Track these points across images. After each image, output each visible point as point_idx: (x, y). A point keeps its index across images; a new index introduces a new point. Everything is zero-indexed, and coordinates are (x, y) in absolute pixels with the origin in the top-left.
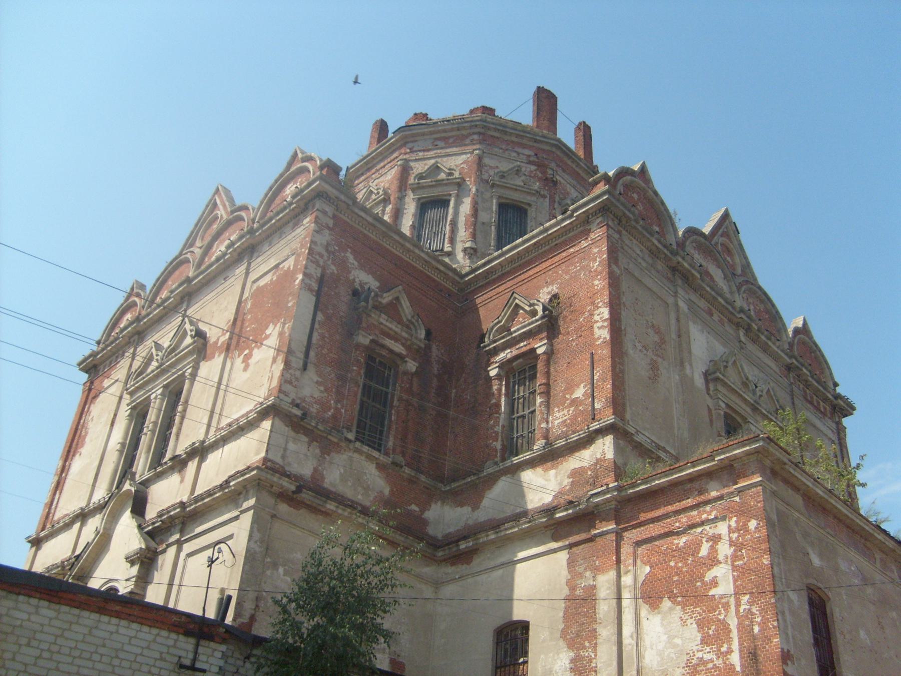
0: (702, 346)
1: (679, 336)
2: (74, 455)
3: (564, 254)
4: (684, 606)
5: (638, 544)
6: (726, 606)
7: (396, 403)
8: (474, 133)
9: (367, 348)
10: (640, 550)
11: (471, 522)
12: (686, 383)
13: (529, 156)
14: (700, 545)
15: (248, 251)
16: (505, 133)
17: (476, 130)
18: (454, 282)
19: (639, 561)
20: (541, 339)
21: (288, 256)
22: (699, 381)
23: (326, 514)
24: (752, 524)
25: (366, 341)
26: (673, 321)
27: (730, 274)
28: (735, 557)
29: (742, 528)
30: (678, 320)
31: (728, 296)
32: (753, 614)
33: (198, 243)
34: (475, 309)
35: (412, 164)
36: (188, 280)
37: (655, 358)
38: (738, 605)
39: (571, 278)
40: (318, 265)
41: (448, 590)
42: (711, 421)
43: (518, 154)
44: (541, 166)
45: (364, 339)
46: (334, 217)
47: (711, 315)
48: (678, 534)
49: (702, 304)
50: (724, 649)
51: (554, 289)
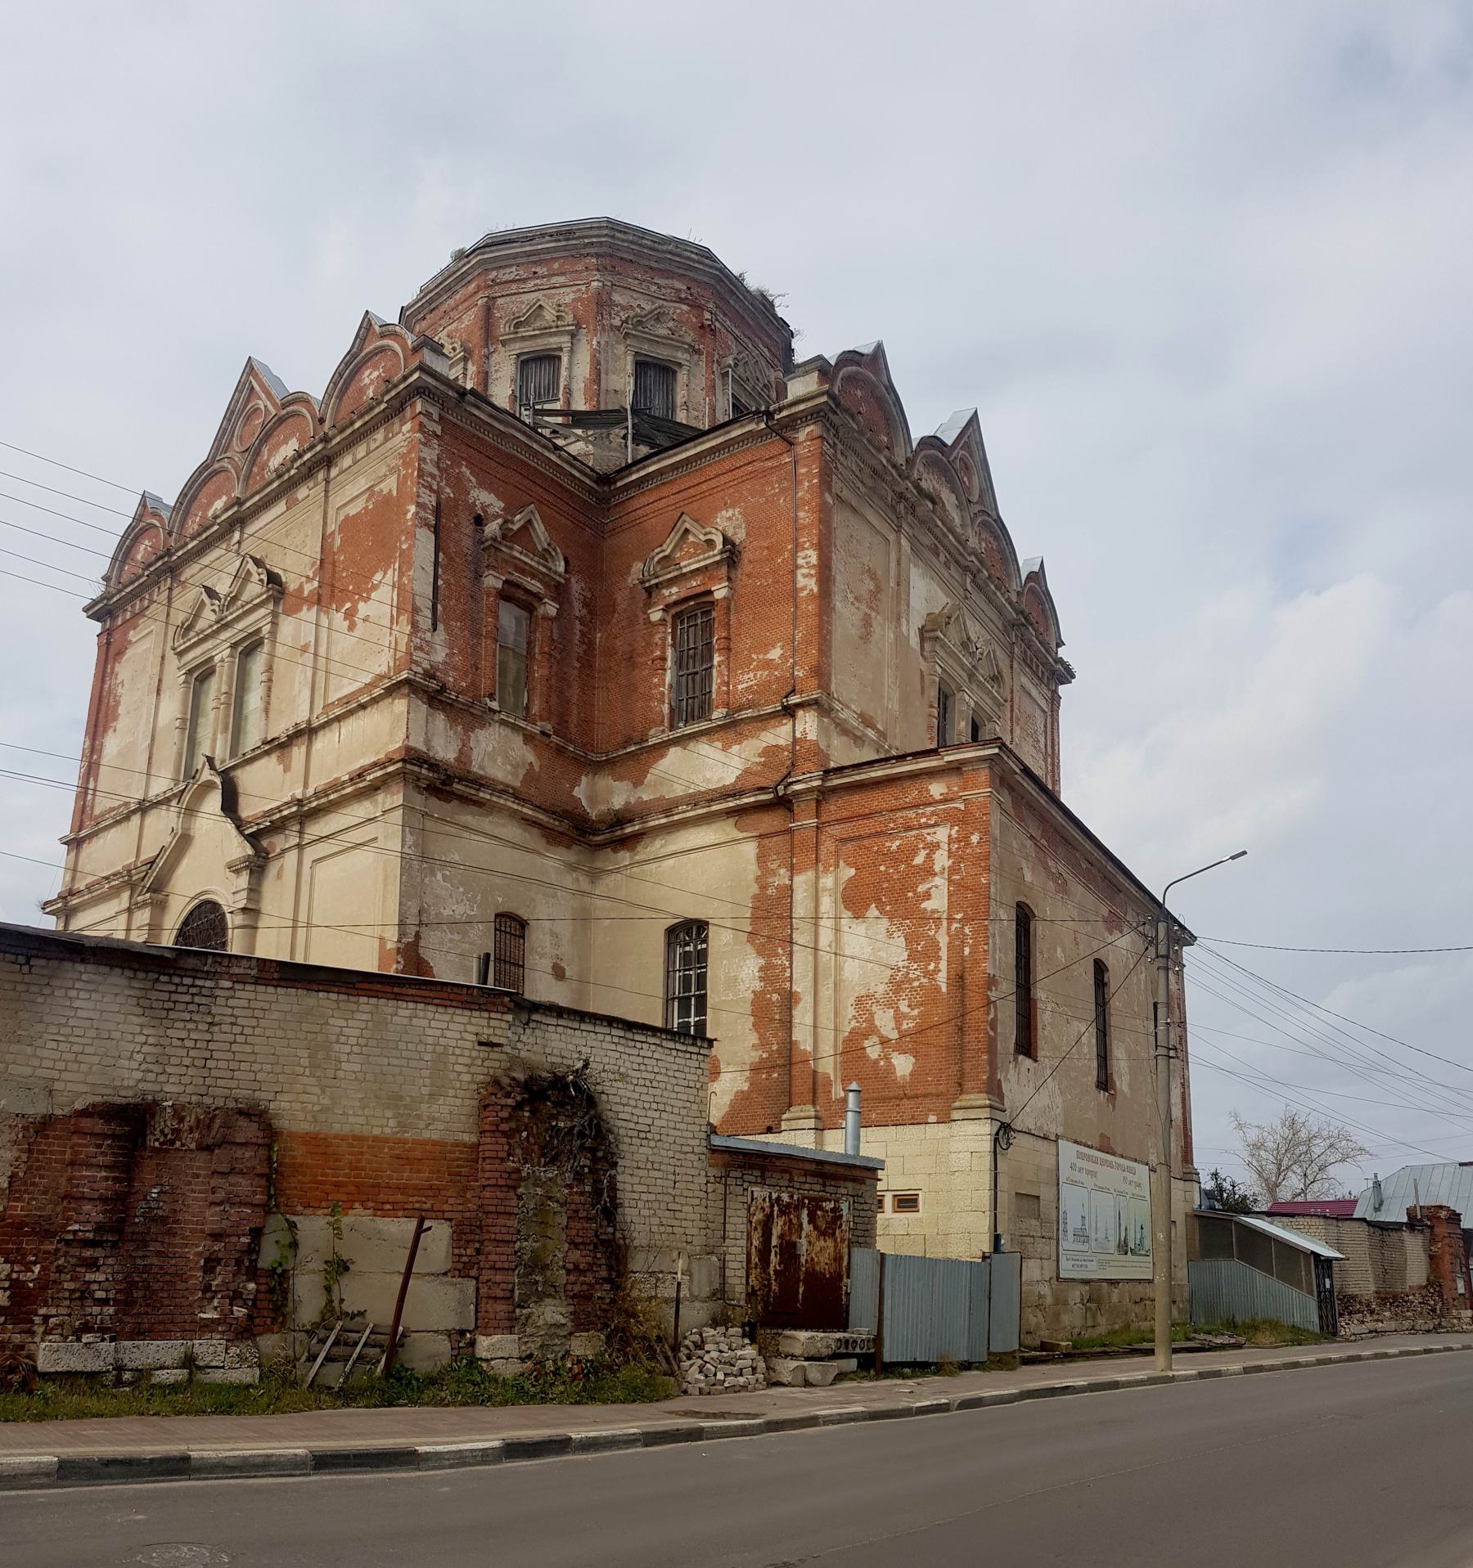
1: (898, 584)
2: (105, 731)
12: (901, 640)
14: (915, 852)
15: (320, 463)
19: (841, 863)
21: (384, 469)
22: (914, 641)
23: (479, 804)
26: (893, 564)
27: (964, 503)
28: (953, 870)
29: (964, 839)
30: (899, 563)
31: (959, 530)
32: (965, 935)
33: (236, 446)
34: (912, 1074)
36: (239, 502)
37: (868, 611)
40: (431, 490)
42: (923, 688)
47: (937, 555)
49: (928, 540)
50: (932, 967)
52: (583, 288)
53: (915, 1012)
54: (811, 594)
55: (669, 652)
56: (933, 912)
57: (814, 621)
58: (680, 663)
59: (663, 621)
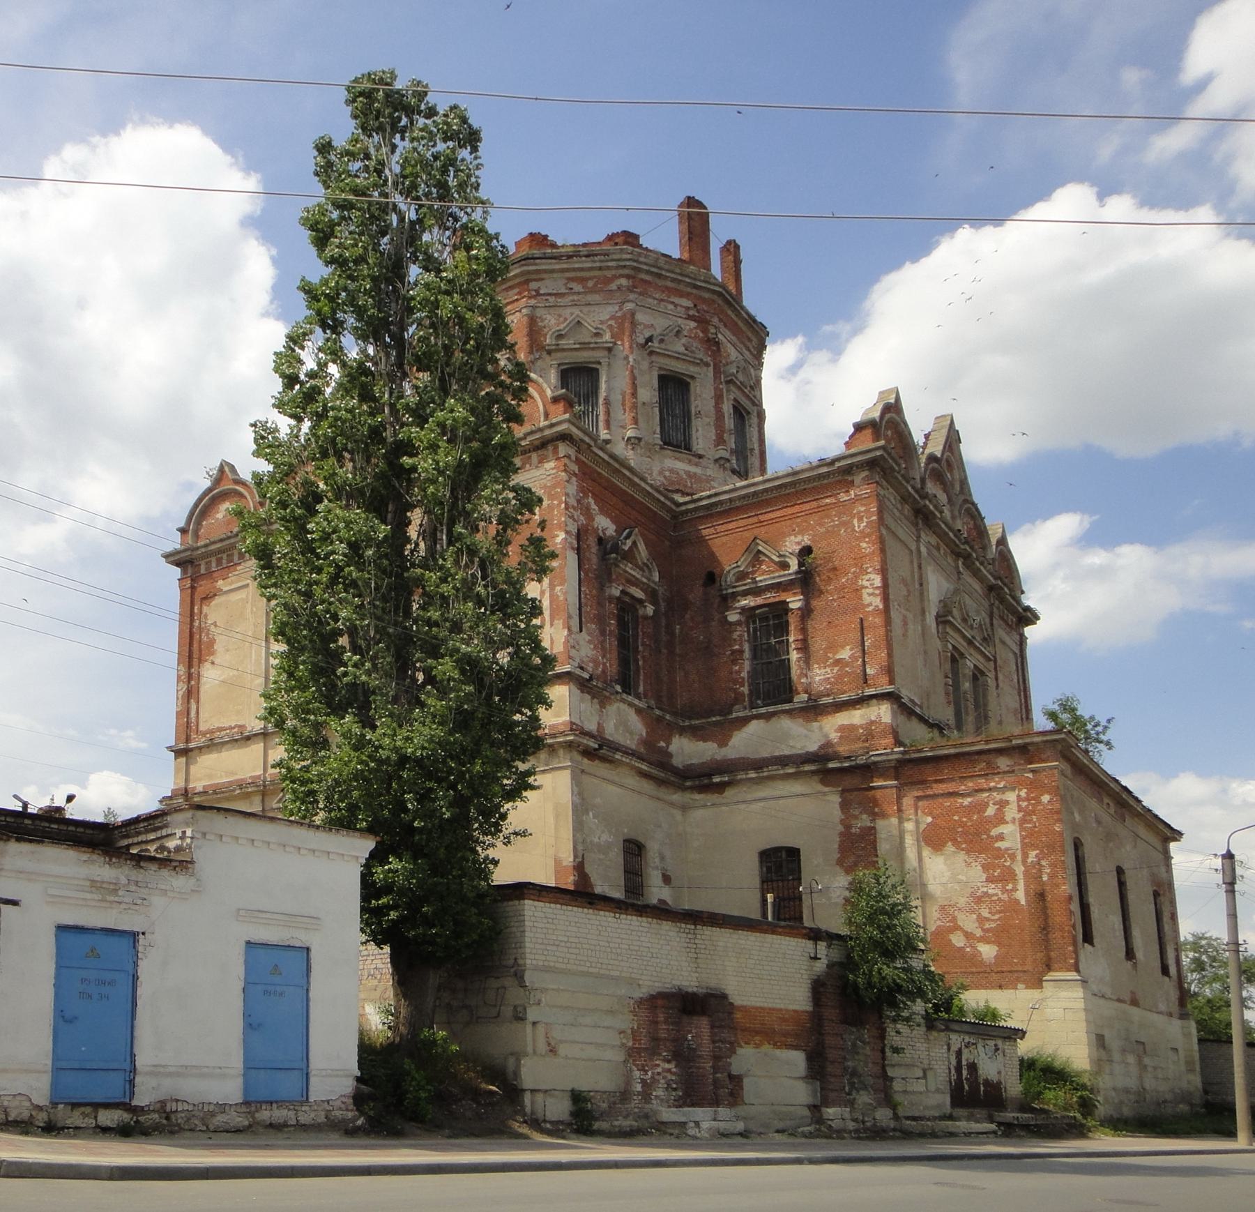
0: (937, 585)
3: (815, 504)
4: (968, 852)
5: (918, 798)
6: (1013, 857)
7: (641, 648)
8: (622, 276)
9: (618, 599)
10: (920, 804)
11: (718, 758)
13: (688, 308)
14: (986, 805)
16: (659, 276)
17: (626, 272)
18: (669, 510)
20: (795, 594)
24: (1046, 798)
25: (616, 593)
35: (539, 312)
38: (1025, 856)
39: (828, 531)
41: (699, 814)
43: (676, 306)
44: (702, 322)
45: (616, 592)
46: (578, 461)
48: (963, 795)
50: (1010, 887)
51: (806, 540)
52: (617, 308)
53: (997, 917)
54: (876, 609)
55: (746, 647)
56: (1007, 849)
57: (882, 631)
58: (755, 656)
59: (739, 623)
